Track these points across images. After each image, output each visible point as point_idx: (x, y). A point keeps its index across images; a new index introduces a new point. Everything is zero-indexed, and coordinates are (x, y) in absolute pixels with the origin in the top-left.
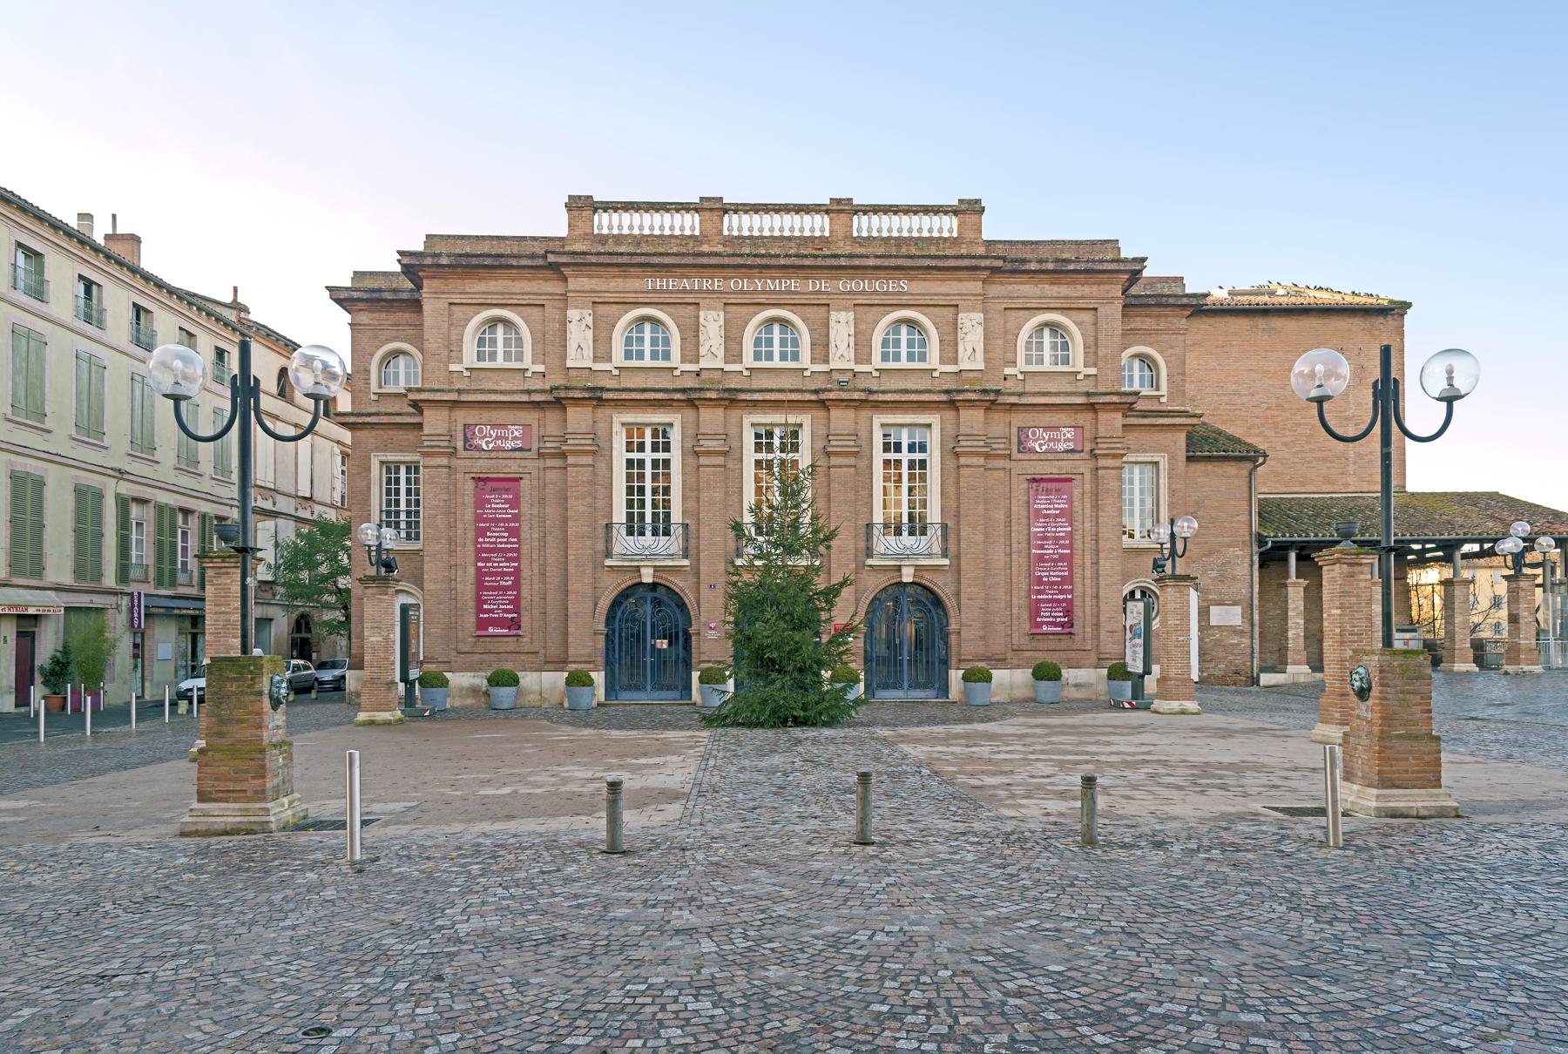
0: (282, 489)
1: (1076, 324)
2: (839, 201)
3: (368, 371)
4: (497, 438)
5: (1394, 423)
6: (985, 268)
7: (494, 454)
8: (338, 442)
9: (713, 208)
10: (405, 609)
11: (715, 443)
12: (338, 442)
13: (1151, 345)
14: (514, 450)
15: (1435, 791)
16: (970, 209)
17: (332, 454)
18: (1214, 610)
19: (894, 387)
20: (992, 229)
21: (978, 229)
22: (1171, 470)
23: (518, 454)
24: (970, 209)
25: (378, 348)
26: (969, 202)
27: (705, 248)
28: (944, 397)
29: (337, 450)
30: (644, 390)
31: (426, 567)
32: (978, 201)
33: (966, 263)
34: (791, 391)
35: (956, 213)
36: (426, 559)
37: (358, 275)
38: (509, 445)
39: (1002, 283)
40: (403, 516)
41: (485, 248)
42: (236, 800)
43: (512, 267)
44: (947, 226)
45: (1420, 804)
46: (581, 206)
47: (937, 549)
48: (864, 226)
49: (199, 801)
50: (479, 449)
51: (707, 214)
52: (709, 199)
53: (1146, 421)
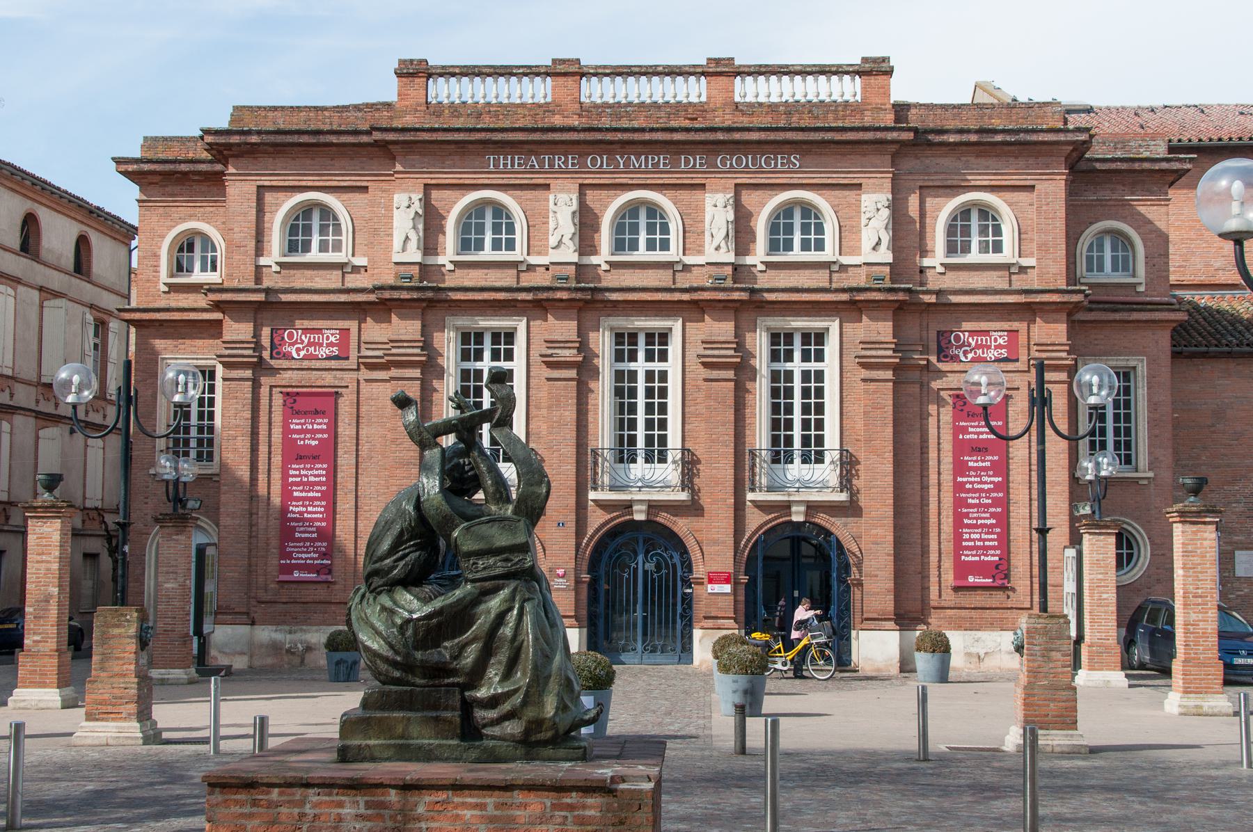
0: (22, 376)
1: (1010, 204)
2: (717, 61)
3: (156, 256)
4: (310, 344)
5: (1047, 422)
6: (893, 142)
7: (306, 364)
8: (92, 307)
9: (568, 71)
10: (201, 551)
11: (567, 352)
12: (92, 307)
13: (1123, 219)
14: (329, 358)
15: (1070, 732)
16: (875, 70)
17: (84, 323)
18: (1240, 556)
19: (782, 285)
20: (901, 89)
21: (887, 95)
22: (1151, 377)
23: (333, 364)
24: (875, 70)
25: (170, 228)
26: (875, 60)
27: (558, 121)
28: (844, 297)
29: (90, 318)
30: (482, 289)
31: (223, 498)
32: (885, 60)
33: (869, 136)
34: (657, 290)
35: (860, 73)
36: (224, 488)
37: (150, 142)
38: (324, 351)
39: (917, 157)
40: (194, 432)
41: (296, 123)
42: (113, 720)
43: (331, 145)
44: (848, 90)
45: (1055, 743)
46: (414, 72)
47: (834, 480)
48: (748, 90)
49: (87, 720)
50: (288, 356)
51: (561, 80)
52: (563, 61)
53: (1117, 316)
